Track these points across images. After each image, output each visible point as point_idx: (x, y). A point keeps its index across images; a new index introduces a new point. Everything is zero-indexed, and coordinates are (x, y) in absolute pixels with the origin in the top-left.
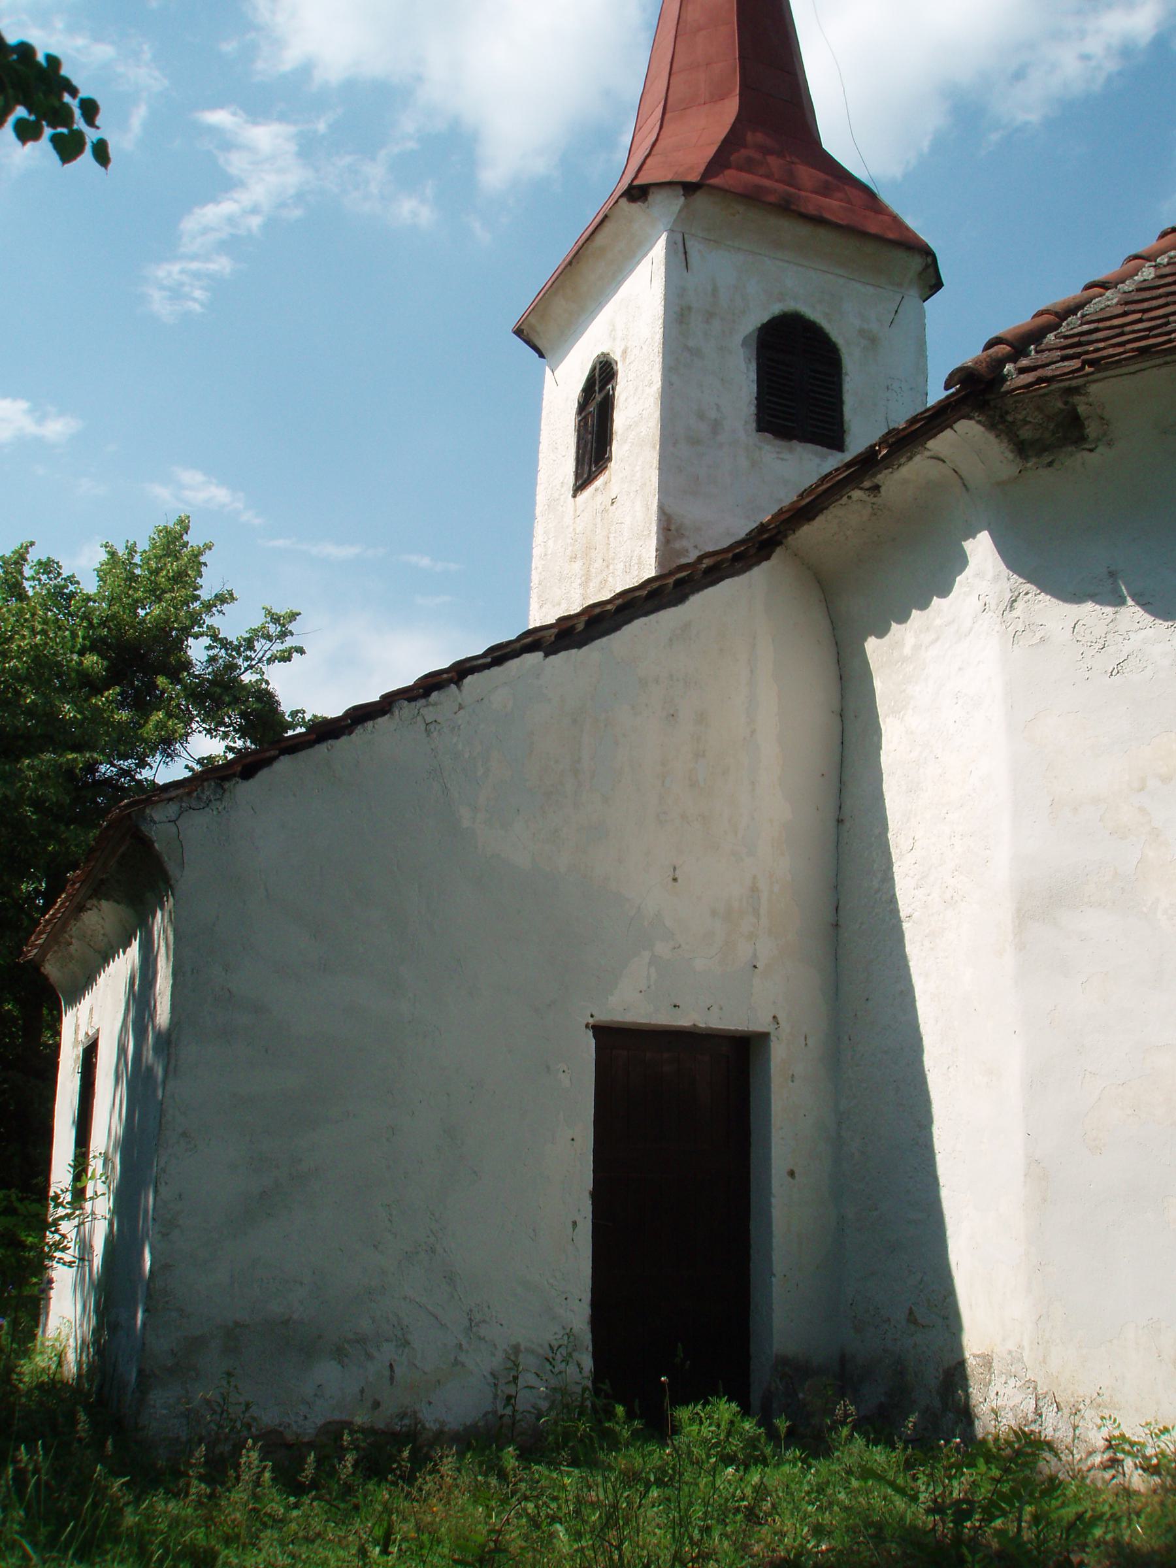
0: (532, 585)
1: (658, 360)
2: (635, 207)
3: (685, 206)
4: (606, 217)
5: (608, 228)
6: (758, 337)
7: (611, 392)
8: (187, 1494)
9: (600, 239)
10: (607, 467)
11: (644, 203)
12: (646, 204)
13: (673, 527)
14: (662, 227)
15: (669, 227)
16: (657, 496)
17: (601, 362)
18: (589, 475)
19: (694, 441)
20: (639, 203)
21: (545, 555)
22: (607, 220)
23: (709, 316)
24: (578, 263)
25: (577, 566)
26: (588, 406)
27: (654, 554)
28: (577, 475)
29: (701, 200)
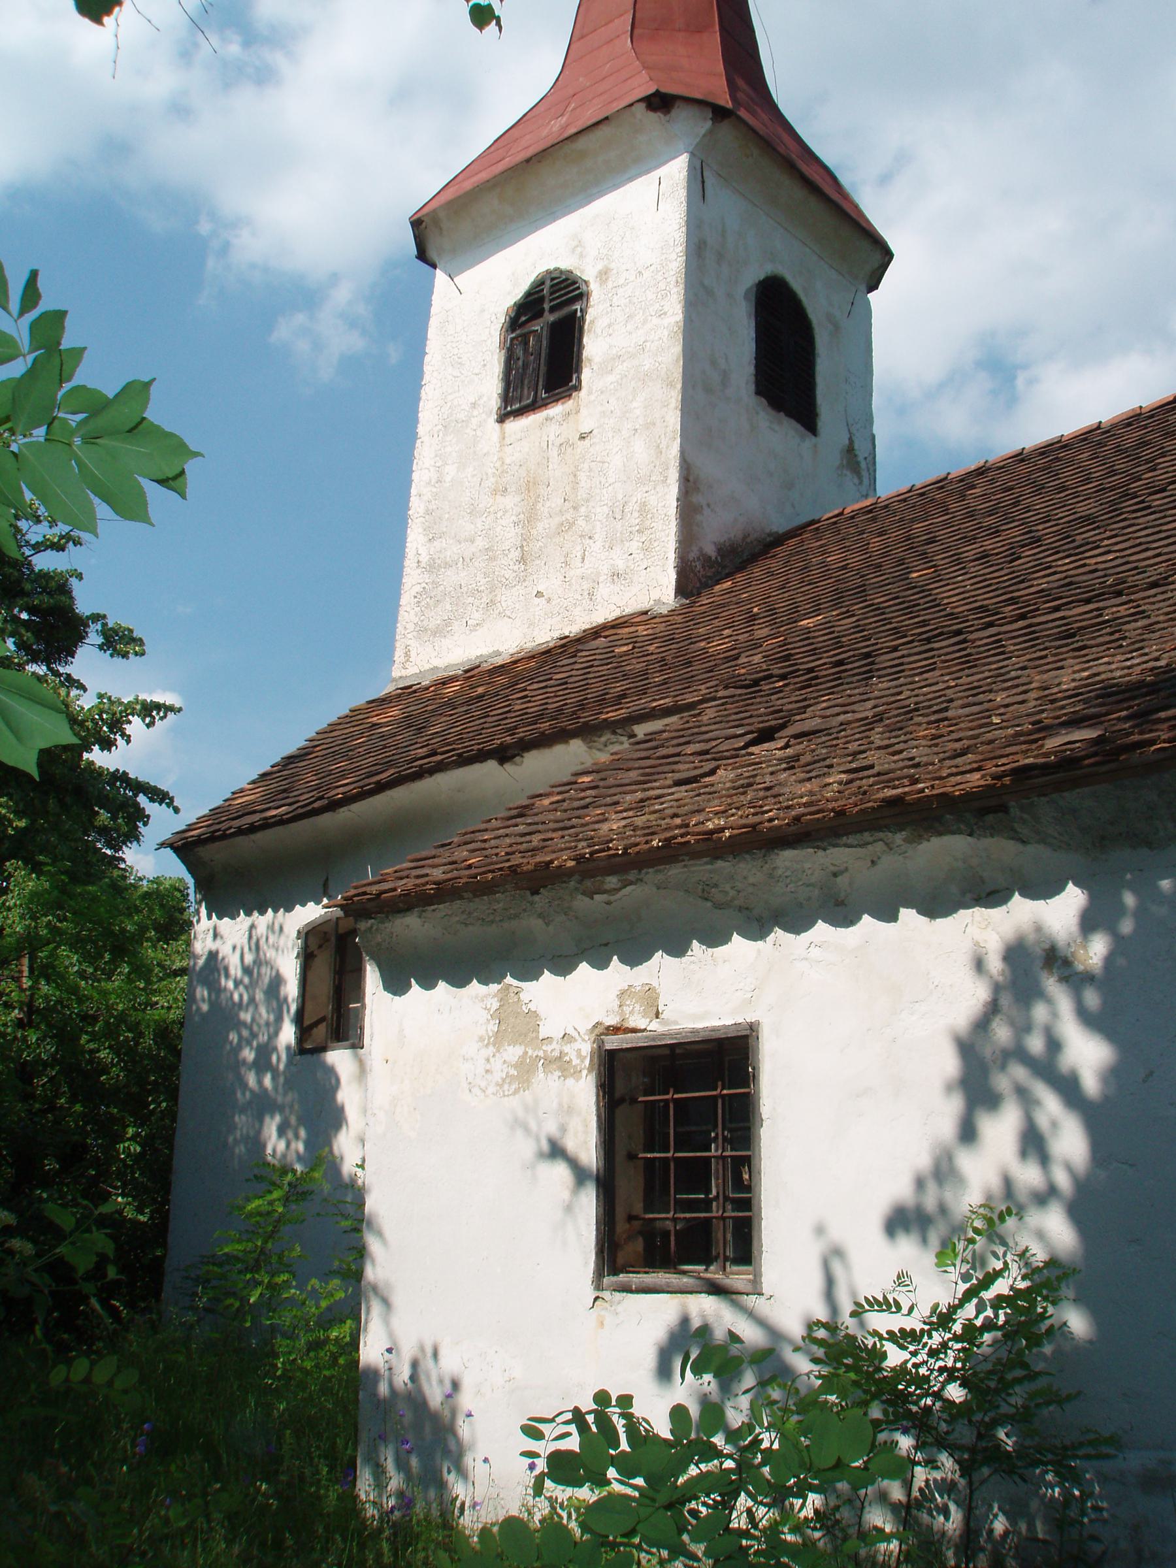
0: (410, 512)
1: (675, 290)
2: (654, 117)
3: (710, 132)
4: (607, 118)
5: (604, 131)
6: (757, 290)
7: (579, 314)
8: (851, 1537)
9: (582, 143)
10: (570, 396)
11: (665, 115)
12: (667, 117)
13: (691, 479)
14: (681, 146)
15: (690, 149)
16: (679, 440)
17: (553, 279)
18: (534, 401)
19: (708, 390)
20: (659, 114)
21: (439, 481)
22: (607, 121)
23: (720, 257)
24: (539, 162)
25: (509, 502)
26: (533, 322)
27: (675, 504)
28: (506, 398)
29: (726, 130)
